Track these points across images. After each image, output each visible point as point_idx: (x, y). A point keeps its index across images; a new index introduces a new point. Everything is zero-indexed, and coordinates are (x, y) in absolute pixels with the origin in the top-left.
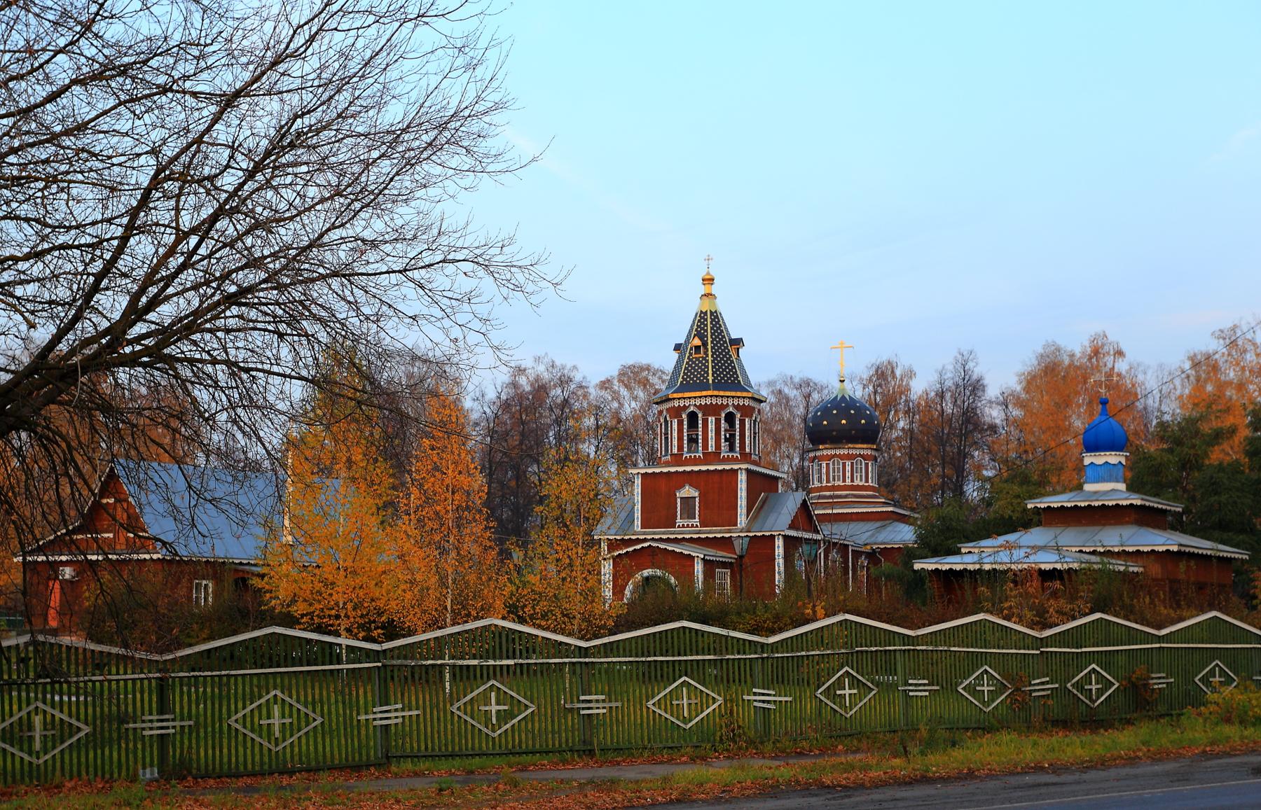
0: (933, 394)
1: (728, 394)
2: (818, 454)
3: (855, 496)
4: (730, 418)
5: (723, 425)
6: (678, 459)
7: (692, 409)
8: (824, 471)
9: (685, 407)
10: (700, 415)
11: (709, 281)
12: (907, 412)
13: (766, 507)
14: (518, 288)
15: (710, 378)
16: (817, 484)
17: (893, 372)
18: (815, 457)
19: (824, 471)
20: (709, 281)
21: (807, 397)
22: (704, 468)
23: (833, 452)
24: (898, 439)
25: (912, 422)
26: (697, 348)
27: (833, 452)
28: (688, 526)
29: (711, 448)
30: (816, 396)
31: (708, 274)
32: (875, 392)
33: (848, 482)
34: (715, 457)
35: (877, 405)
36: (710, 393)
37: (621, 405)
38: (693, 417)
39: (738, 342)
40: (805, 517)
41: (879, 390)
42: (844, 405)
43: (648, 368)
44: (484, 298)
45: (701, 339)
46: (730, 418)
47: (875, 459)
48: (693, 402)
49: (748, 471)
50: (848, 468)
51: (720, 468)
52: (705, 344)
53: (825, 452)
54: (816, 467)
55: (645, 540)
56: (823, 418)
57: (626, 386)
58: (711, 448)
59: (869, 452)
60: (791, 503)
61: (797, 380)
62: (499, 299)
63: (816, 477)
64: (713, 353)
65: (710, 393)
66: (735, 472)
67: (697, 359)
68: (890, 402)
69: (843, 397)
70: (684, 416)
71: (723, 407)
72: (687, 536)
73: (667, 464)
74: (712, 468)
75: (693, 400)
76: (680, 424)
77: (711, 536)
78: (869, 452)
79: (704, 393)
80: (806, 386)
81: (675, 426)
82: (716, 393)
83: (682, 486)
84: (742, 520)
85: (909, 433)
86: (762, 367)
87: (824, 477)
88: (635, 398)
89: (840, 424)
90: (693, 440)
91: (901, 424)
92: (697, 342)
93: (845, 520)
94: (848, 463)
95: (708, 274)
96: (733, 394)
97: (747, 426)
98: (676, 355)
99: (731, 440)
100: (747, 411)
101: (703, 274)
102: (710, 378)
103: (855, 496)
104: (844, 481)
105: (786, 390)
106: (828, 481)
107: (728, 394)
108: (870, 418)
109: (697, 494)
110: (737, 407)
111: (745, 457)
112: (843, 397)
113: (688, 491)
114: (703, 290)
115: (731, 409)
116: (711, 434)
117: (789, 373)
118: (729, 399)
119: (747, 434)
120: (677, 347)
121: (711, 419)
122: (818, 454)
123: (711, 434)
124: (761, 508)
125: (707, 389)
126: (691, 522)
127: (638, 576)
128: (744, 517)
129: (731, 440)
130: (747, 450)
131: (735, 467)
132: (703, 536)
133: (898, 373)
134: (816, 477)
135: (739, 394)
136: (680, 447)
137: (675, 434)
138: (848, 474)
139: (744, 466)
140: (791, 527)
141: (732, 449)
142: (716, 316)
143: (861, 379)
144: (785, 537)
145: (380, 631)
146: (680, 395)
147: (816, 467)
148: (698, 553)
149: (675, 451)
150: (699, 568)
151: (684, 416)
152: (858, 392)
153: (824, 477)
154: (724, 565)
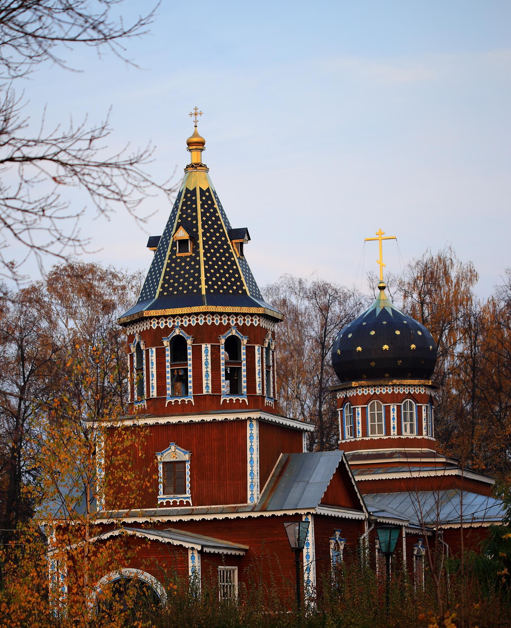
0: (503, 304)
1: (229, 309)
2: (350, 394)
3: (406, 455)
4: (233, 345)
5: (223, 355)
6: (157, 407)
7: (177, 332)
8: (359, 418)
9: (167, 331)
10: (189, 342)
11: (196, 145)
12: (466, 331)
13: (286, 474)
14: (120, 197)
15: (203, 287)
16: (348, 438)
17: (446, 273)
18: (346, 399)
19: (359, 418)
20: (196, 145)
21: (325, 309)
22: (197, 419)
23: (371, 391)
24: (453, 370)
25: (474, 344)
26: (183, 243)
27: (371, 391)
28: (176, 505)
29: (207, 390)
30: (336, 309)
31: (196, 135)
32: (422, 302)
33: (394, 434)
34: (210, 402)
35: (424, 321)
36: (202, 309)
37: (53, 325)
38: (178, 345)
39: (241, 235)
40: (343, 488)
41: (428, 299)
42: (381, 322)
43: (92, 269)
44: (73, 210)
45: (188, 230)
46: (233, 345)
47: (431, 400)
48: (178, 322)
49: (260, 421)
50: (393, 414)
51: (220, 418)
52: (194, 237)
53: (360, 392)
54: (347, 414)
55: (111, 527)
56: (355, 342)
57: (61, 297)
58: (207, 390)
59: (422, 391)
60: (323, 469)
61: (308, 285)
62: (92, 211)
63: (347, 427)
64: (206, 251)
65: (202, 309)
66: (242, 424)
67: (183, 259)
68: (443, 317)
69: (384, 311)
70: (166, 343)
71: (223, 329)
72: (174, 519)
73: (143, 413)
74: (208, 418)
75: (179, 320)
76: (161, 354)
77: (209, 517)
78: (422, 391)
79: (195, 309)
80: (323, 296)
81: (153, 358)
82: (212, 309)
83: (166, 446)
84: (254, 494)
85: (470, 362)
86: (273, 265)
87: (359, 428)
88: (73, 315)
89: (379, 349)
90: (180, 378)
91: (459, 348)
92: (182, 234)
93: (390, 490)
94: (393, 407)
95: (196, 135)
96: (237, 309)
97: (257, 356)
98: (150, 255)
99: (233, 376)
100: (256, 335)
101: (188, 134)
102: (203, 287)
103: (406, 455)
104: (388, 433)
105: (293, 300)
106: (365, 434)
107: (229, 309)
108: (423, 342)
109: (187, 457)
110: (243, 329)
111: (256, 402)
112: (384, 311)
113: (174, 453)
114: (188, 158)
115: (234, 332)
116: (207, 369)
117: (297, 276)
118: (231, 319)
119: (258, 368)
120: (153, 242)
121: (206, 348)
122: (350, 394)
123: (207, 369)
124: (280, 474)
125: (200, 303)
126: (179, 498)
127: (104, 579)
128: (256, 490)
129: (233, 376)
130: (259, 391)
131: (243, 416)
132: (197, 518)
133: (453, 274)
134: (347, 427)
135: (245, 310)
136: (161, 389)
137: (153, 370)
138: (393, 423)
139: (255, 415)
140: (325, 503)
141: (235, 389)
142: (208, 196)
143: (401, 283)
144: (316, 517)
145: (117, 596)
146: (160, 312)
147: (347, 414)
148: (193, 544)
149: (154, 393)
150: (194, 563)
151: (166, 343)
152: (398, 303)
153: (359, 428)
154: (230, 560)
